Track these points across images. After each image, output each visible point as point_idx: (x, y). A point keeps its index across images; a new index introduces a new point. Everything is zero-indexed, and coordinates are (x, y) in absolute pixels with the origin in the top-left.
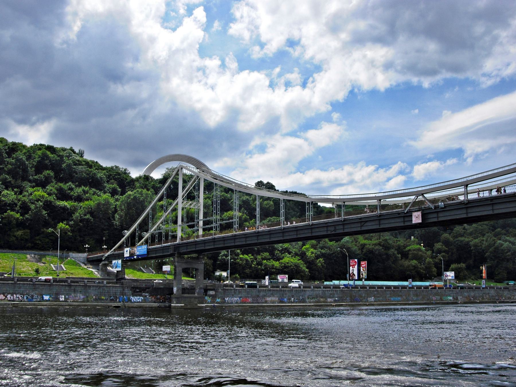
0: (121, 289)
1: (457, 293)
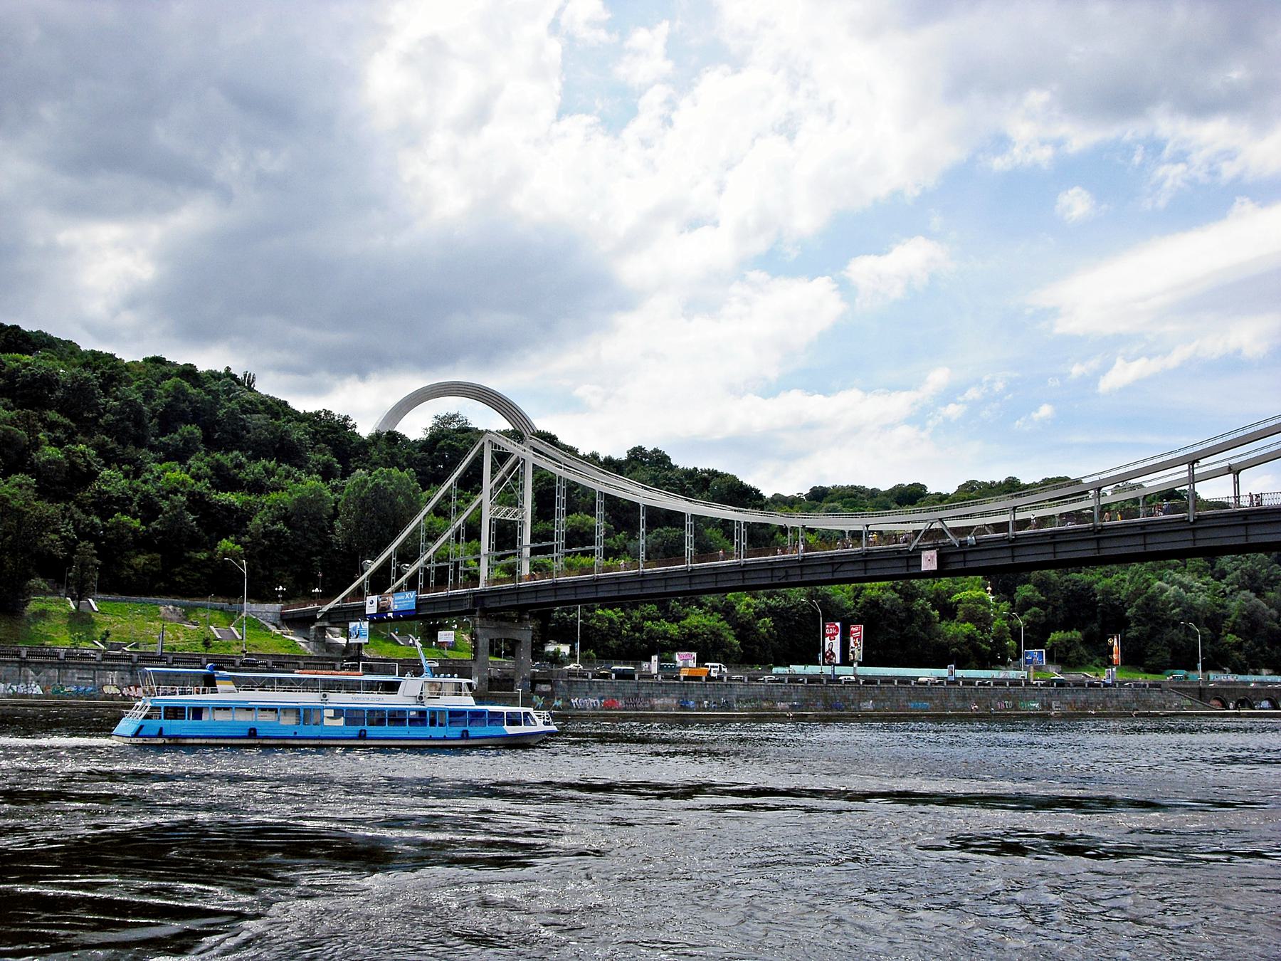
1: (1050, 694)
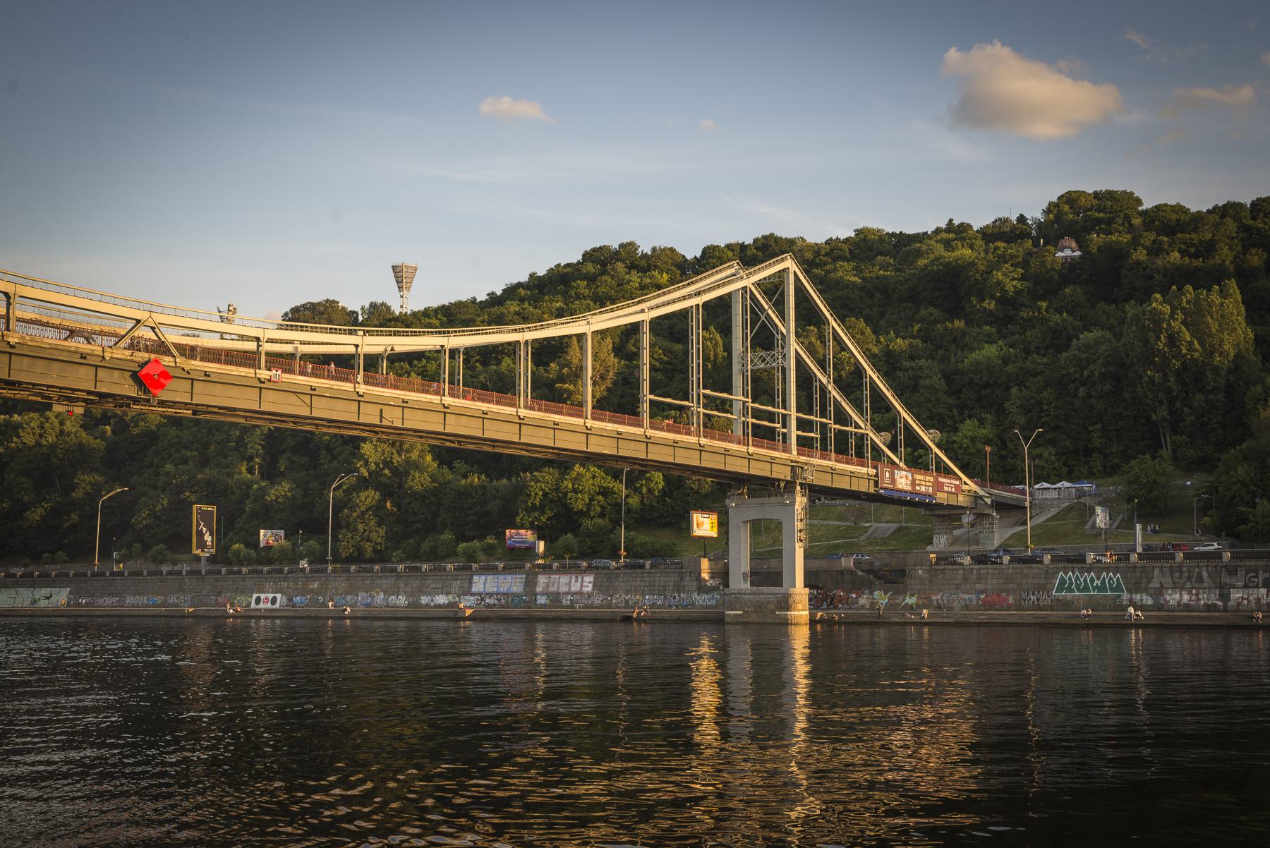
0: (677, 579)
